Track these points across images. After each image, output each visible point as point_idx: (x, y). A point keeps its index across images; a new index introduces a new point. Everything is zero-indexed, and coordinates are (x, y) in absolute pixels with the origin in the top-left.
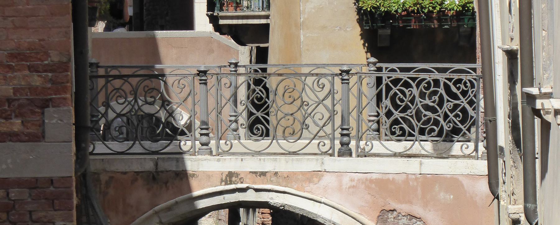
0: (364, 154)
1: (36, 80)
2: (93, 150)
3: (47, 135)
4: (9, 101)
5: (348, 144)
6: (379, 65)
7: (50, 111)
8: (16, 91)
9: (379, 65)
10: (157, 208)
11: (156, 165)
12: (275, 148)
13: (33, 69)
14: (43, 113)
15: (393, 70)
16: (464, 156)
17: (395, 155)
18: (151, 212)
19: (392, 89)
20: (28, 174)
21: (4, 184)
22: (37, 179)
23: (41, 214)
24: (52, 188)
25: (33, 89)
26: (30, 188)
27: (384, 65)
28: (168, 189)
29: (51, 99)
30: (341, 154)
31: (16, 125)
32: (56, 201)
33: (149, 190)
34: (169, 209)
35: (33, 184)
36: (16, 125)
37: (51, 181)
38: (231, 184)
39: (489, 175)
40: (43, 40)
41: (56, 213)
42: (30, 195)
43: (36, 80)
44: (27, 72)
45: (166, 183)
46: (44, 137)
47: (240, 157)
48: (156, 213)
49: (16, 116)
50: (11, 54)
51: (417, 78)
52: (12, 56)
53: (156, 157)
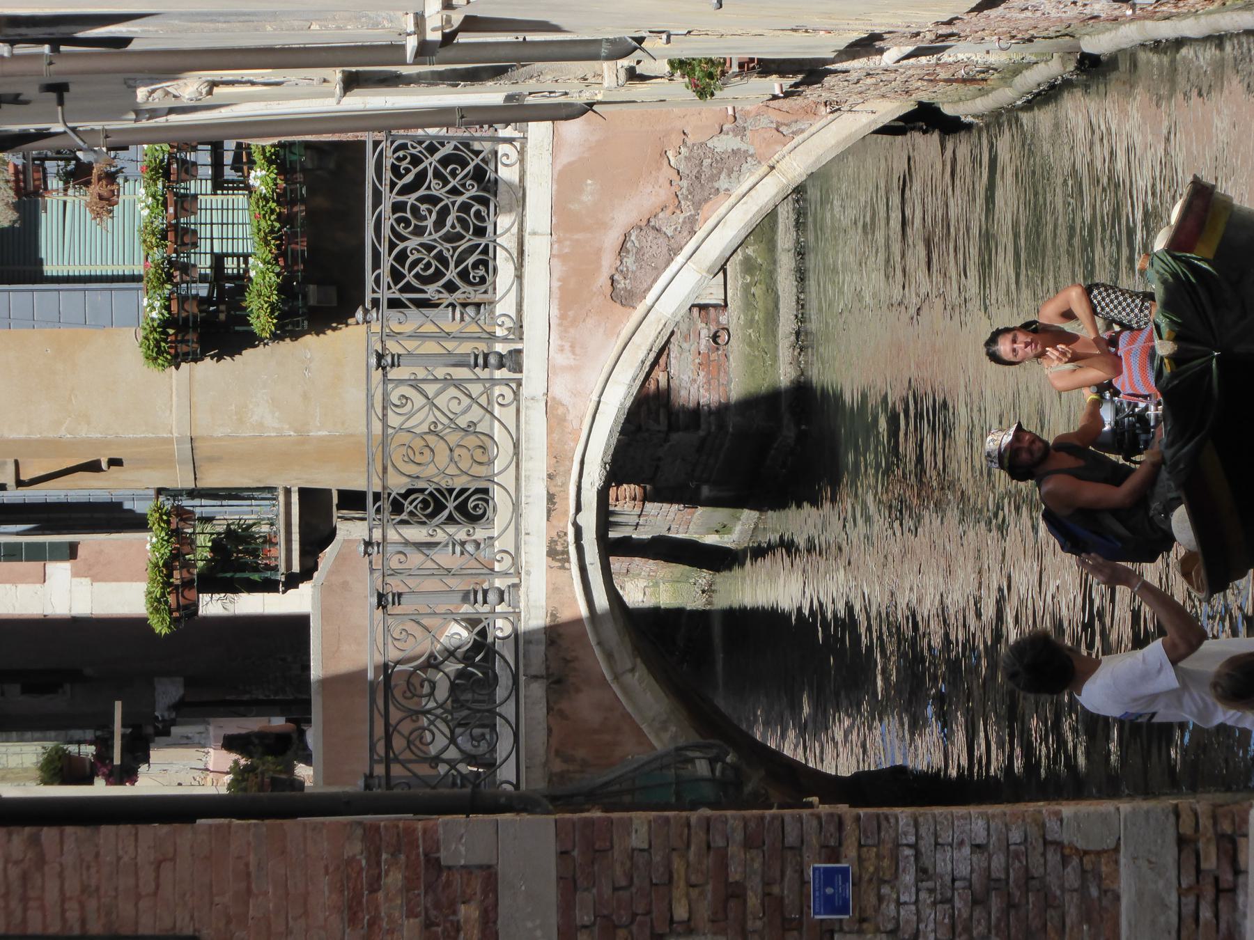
0: (518, 329)
1: (394, 879)
3: (485, 861)
4: (428, 924)
5: (501, 356)
6: (368, 305)
9: (368, 305)
10: (608, 677)
11: (535, 677)
12: (507, 479)
14: (449, 868)
15: (377, 281)
16: (522, 161)
17: (519, 277)
18: (615, 687)
21: (567, 934)
22: (560, 878)
25: (409, 885)
28: (576, 659)
29: (426, 855)
30: (518, 368)
31: (468, 913)
32: (597, 847)
33: (578, 690)
34: (609, 656)
35: (569, 885)
36: (468, 913)
37: (563, 854)
40: (326, 867)
41: (616, 847)
43: (394, 879)
45: (566, 661)
46: (489, 867)
48: (616, 677)
53: (522, 678)
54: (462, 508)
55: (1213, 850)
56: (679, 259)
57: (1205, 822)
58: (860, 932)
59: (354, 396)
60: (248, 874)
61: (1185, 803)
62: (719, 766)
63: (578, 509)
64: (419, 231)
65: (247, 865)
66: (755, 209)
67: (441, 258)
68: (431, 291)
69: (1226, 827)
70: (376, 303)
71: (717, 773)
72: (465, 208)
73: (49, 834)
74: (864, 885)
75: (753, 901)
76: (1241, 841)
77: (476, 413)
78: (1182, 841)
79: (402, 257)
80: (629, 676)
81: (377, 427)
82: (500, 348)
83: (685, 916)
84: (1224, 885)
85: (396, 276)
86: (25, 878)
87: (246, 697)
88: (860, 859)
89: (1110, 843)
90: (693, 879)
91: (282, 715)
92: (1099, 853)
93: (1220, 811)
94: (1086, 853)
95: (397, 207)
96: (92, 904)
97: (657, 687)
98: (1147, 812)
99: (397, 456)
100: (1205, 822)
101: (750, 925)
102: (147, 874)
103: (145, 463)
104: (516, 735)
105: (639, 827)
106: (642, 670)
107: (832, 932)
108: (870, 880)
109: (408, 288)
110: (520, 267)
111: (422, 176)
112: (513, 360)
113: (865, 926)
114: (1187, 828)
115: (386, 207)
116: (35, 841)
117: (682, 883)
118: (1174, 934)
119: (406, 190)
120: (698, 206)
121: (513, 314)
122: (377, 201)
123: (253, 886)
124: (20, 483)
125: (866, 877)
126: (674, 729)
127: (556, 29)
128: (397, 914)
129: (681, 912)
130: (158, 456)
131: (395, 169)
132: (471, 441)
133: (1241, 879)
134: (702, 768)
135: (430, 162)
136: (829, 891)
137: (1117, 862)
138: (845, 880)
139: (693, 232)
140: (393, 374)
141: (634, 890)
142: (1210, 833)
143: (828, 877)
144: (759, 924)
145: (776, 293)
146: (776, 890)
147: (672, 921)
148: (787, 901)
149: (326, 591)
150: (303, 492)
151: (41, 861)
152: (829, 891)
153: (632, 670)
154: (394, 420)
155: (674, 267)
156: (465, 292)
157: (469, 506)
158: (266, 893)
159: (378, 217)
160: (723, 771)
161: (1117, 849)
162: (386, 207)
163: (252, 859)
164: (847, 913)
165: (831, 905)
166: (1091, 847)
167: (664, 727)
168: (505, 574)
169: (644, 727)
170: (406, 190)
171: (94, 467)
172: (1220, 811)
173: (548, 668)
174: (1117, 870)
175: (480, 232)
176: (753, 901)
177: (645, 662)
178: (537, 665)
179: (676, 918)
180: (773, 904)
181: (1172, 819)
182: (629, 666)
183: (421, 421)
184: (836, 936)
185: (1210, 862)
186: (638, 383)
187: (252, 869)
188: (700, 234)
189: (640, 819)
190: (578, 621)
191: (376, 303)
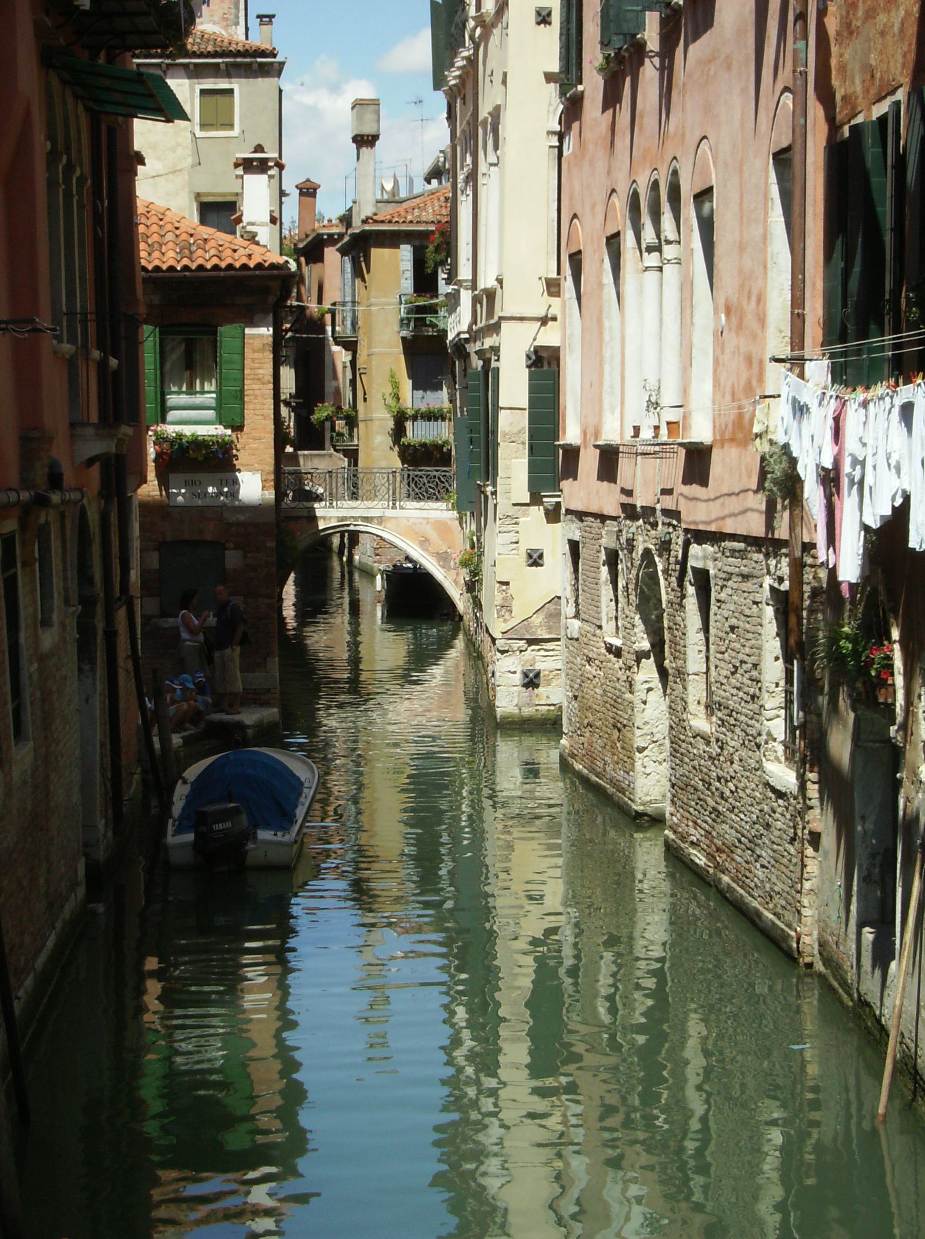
0: (402, 508)
30: (392, 508)
54: (354, 493)
59: (384, 464)
61: (278, 691)
63: (355, 525)
64: (429, 482)
67: (420, 488)
68: (412, 485)
72: (435, 494)
73: (271, 386)
77: (380, 497)
79: (421, 477)
81: (375, 470)
82: (398, 503)
85: (416, 476)
86: (259, 379)
95: (435, 477)
96: (252, 397)
99: (368, 476)
102: (260, 412)
103: (365, 407)
105: (272, 544)
109: (413, 479)
111: (443, 482)
112: (394, 507)
115: (435, 473)
116: (269, 382)
119: (439, 478)
122: (437, 471)
124: (360, 374)
127: (368, 272)
130: (367, 411)
131: (444, 476)
132: (372, 495)
135: (447, 485)
140: (391, 476)
150: (357, 450)
151: (263, 384)
154: (378, 475)
156: (412, 493)
157: (354, 496)
159: (432, 471)
162: (435, 473)
170: (439, 478)
171: (365, 394)
175: (428, 498)
183: (377, 482)
189: (273, 544)
190: (317, 526)
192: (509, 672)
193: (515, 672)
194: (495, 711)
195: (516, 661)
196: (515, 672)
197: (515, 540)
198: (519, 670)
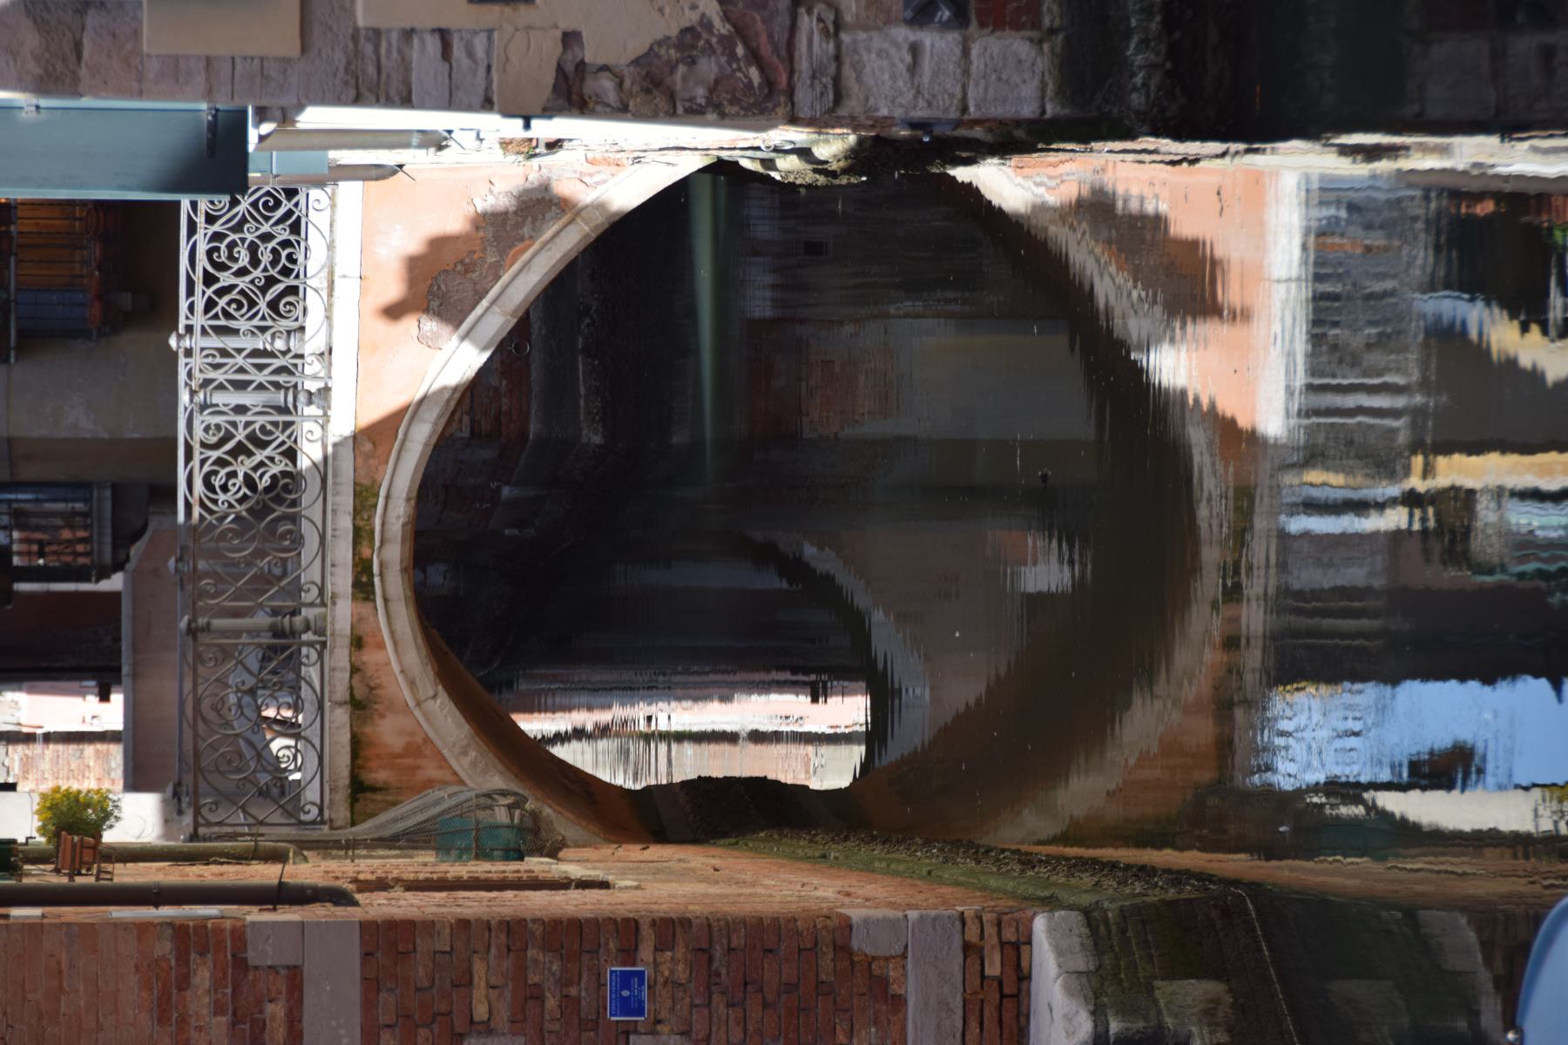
0: (326, 354)
1: (203, 976)
2: (313, 804)
3: (292, 962)
4: (236, 1022)
5: (310, 393)
6: (181, 330)
7: (252, 957)
8: (218, 1010)
9: (181, 330)
10: (411, 704)
11: (340, 704)
12: (316, 513)
13: (184, 982)
14: (256, 968)
15: (191, 308)
16: (333, 206)
17: (328, 318)
18: (417, 713)
19: (240, 442)
20: (354, 992)
21: (370, 1036)
22: (365, 979)
23: (421, 972)
24: (379, 954)
25: (217, 985)
26: (379, 990)
27: (182, 323)
28: (379, 686)
29: (233, 955)
30: (326, 408)
31: (276, 1011)
32: (400, 949)
33: (382, 716)
34: (412, 684)
35: (371, 986)
36: (276, 1011)
37: (367, 955)
38: (372, 585)
39: (364, 179)
40: (136, 966)
41: (419, 949)
42: (391, 990)
43: (203, 976)
44: (189, 993)
45: (372, 689)
46: (296, 967)
47: (328, 569)
48: (418, 704)
49: (261, 1011)
50: (159, 1021)
51: (205, 270)
52: (162, 1017)
53: (327, 704)
55: (997, 957)
56: (485, 303)
57: (990, 930)
58: (653, 1033)
60: (60, 972)
62: (517, 813)
65: (59, 963)
66: (558, 255)
69: (1009, 935)
70: (189, 329)
71: (516, 821)
74: (659, 987)
75: (551, 1002)
76: (1024, 949)
78: (967, 948)
80: (431, 702)
83: (486, 1017)
84: (1007, 991)
87: (59, 664)
88: (656, 964)
89: (897, 949)
90: (493, 981)
91: (93, 678)
92: (887, 959)
93: (1005, 918)
94: (874, 958)
97: (458, 714)
98: (935, 919)
100: (990, 930)
101: (548, 1026)
104: (321, 758)
106: (443, 697)
107: (627, 1034)
108: (665, 983)
110: (329, 309)
113: (659, 1028)
114: (972, 934)
117: (483, 984)
118: (958, 1036)
120: (503, 253)
121: (319, 582)
123: (65, 984)
125: (661, 980)
126: (473, 754)
128: (205, 1012)
129: (481, 1012)
133: (1024, 985)
134: (501, 816)
136: (626, 993)
137: (904, 967)
138: (641, 983)
139: (498, 278)
141: (435, 990)
142: (995, 940)
143: (625, 979)
144: (557, 1027)
145: (584, 846)
146: (573, 991)
147: (472, 1021)
148: (583, 1003)
149: (134, 583)
152: (626, 993)
153: (434, 697)
155: (479, 310)
158: (77, 991)
160: (522, 816)
161: (904, 956)
163: (64, 957)
164: (642, 1014)
165: (631, 1007)
166: (881, 953)
167: (465, 753)
168: (315, 377)
169: (445, 751)
172: (1005, 918)
173: (352, 695)
174: (905, 976)
176: (551, 1002)
177: (446, 688)
178: (341, 692)
179: (476, 1018)
180: (569, 1004)
181: (958, 924)
182: (431, 693)
184: (632, 1038)
185: (993, 968)
186: (443, 421)
187: (64, 967)
188: (505, 278)
191: (189, 329)
192: (914, 68)
193: (915, 49)
194: (1054, 121)
195: (877, 42)
196: (915, 49)
197: (433, 45)
198: (903, 34)
